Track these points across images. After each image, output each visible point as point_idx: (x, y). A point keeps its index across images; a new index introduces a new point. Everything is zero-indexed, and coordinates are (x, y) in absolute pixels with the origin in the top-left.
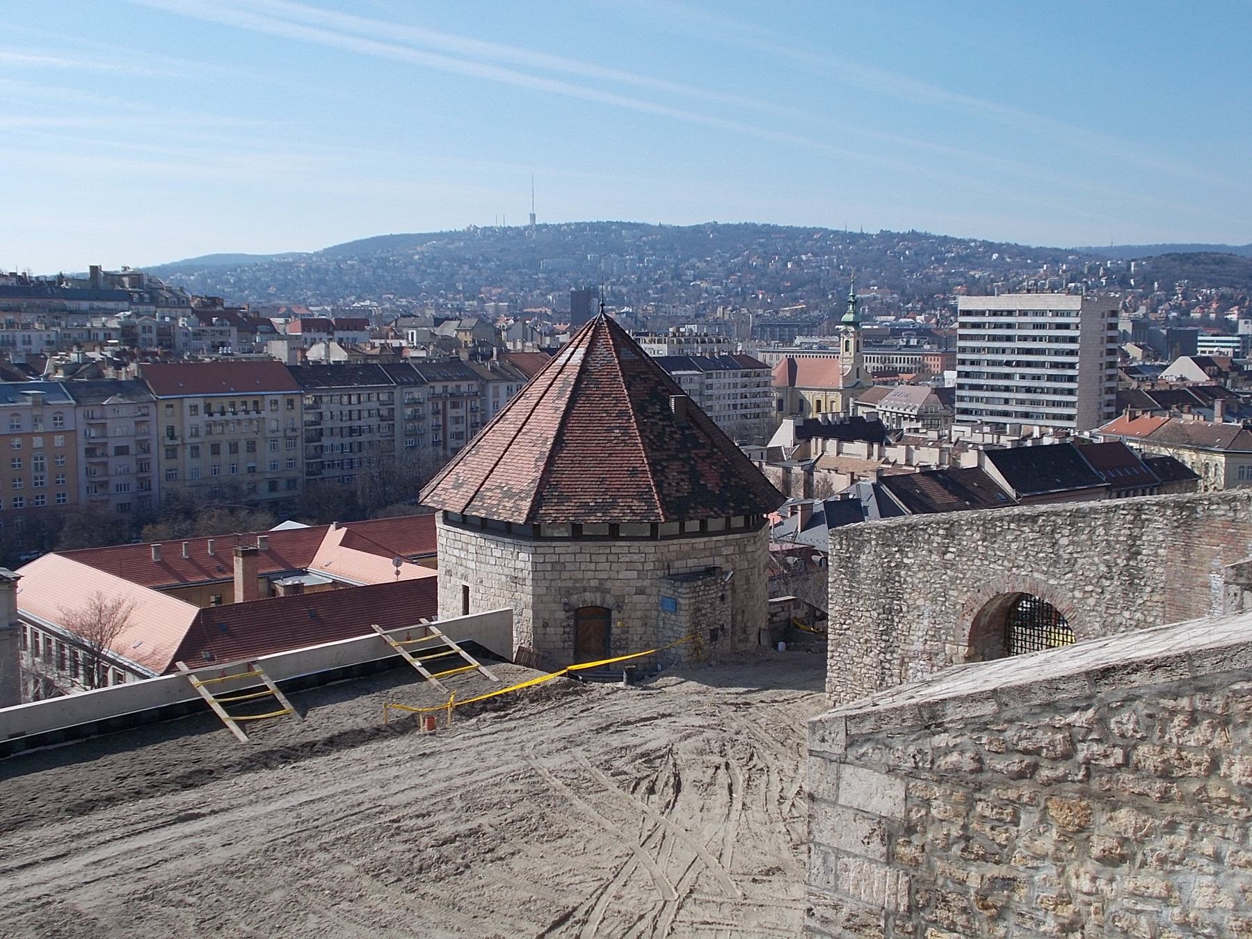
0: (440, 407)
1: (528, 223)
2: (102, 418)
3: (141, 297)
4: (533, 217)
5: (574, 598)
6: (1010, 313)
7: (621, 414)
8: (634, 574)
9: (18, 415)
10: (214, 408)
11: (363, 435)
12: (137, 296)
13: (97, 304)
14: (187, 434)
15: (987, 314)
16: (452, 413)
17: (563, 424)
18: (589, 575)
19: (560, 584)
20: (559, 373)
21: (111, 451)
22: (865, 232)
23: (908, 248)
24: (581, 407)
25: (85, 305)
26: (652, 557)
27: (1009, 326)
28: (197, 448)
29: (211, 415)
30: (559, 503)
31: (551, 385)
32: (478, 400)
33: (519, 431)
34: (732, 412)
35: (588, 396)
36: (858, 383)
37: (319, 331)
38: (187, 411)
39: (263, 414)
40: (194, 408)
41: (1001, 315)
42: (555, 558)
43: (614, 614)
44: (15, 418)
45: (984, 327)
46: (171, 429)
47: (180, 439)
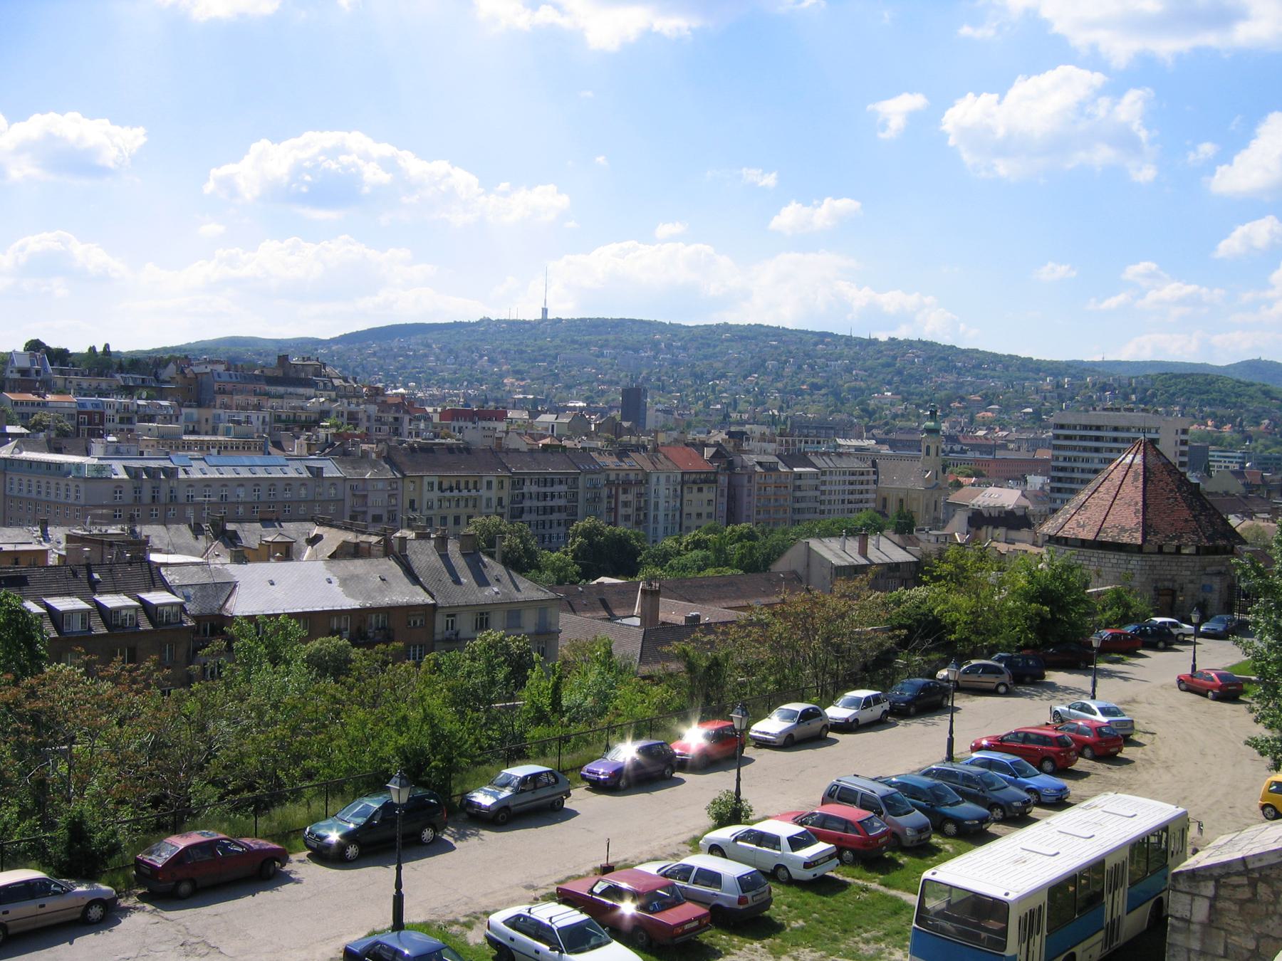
0: (613, 492)
1: (539, 316)
2: (363, 490)
3: (325, 384)
4: (545, 311)
5: (1159, 585)
6: (1098, 428)
7: (1171, 491)
8: (1189, 573)
9: (290, 484)
10: (445, 486)
11: (554, 514)
12: (321, 384)
13: (291, 390)
14: (425, 506)
15: (1078, 428)
16: (622, 497)
17: (1144, 495)
18: (1167, 572)
19: (1152, 576)
20: (1129, 468)
21: (369, 518)
22: (872, 337)
23: (918, 357)
24: (1150, 487)
25: (281, 389)
26: (1198, 564)
27: (1097, 439)
28: (431, 519)
29: (469, 491)
30: (1155, 535)
31: (1126, 474)
32: (643, 488)
33: (1115, 498)
34: (841, 507)
35: (1152, 481)
36: (937, 484)
37: (465, 421)
38: (426, 487)
39: (481, 492)
40: (431, 484)
41: (1091, 429)
42: (1151, 563)
43: (1178, 593)
44: (190, 489)
45: (1075, 439)
46: (412, 502)
47: (419, 511)
